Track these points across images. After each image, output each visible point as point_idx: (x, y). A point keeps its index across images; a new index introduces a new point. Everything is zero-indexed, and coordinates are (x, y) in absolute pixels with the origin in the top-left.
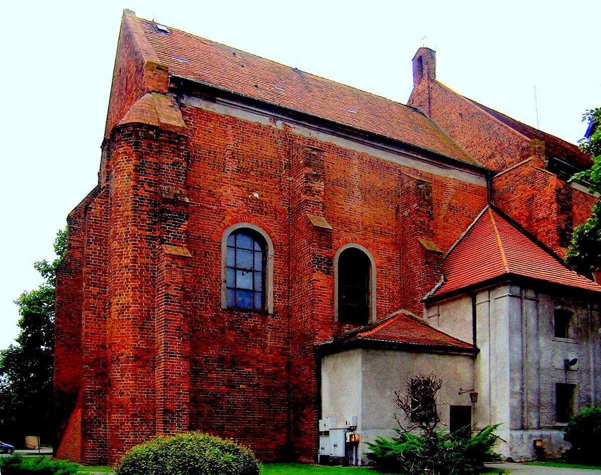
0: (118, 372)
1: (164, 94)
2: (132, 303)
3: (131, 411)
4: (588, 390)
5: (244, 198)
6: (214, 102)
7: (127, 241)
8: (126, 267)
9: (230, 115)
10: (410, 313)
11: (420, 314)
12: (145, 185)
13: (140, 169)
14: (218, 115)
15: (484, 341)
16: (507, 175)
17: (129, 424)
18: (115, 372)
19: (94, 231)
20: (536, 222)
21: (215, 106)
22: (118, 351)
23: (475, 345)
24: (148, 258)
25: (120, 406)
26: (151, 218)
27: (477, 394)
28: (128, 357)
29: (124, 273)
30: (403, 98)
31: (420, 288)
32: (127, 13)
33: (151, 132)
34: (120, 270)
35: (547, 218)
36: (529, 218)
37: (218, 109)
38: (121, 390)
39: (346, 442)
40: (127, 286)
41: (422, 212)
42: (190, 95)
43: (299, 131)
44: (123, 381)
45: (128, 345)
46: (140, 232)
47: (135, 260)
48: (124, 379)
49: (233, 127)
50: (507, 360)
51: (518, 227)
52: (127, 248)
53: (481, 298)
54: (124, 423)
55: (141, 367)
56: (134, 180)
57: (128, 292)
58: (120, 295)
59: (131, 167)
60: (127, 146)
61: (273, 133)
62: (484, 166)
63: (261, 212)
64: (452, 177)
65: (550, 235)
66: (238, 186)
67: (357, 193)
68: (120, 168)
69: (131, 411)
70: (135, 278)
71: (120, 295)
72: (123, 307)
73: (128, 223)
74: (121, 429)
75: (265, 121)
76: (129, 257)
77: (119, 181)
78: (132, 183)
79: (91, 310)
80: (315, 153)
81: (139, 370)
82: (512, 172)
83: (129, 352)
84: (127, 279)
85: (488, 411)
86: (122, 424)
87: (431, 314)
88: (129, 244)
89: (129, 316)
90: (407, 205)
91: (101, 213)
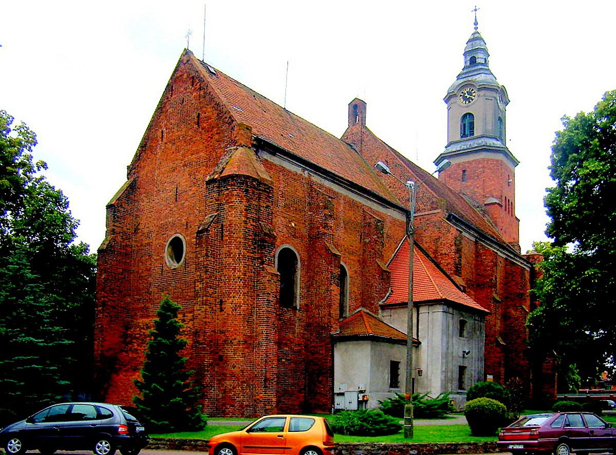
0: (232, 352)
1: (249, 148)
2: (243, 304)
3: (241, 379)
4: (472, 370)
5: (287, 226)
6: (274, 155)
7: (240, 260)
8: (239, 278)
9: (283, 166)
10: (368, 311)
11: (376, 312)
12: (251, 221)
13: (249, 209)
14: (275, 165)
15: (425, 337)
16: (421, 217)
17: (240, 388)
18: (229, 351)
19: (211, 248)
20: (440, 255)
21: (275, 158)
22: (231, 337)
23: (418, 339)
24: (251, 272)
25: (233, 375)
26: (254, 245)
27: (422, 371)
28: (239, 341)
29: (237, 282)
30: (339, 135)
31: (377, 295)
32: (187, 52)
33: (254, 183)
34: (234, 280)
35: (448, 255)
36: (435, 252)
37: (276, 160)
38: (234, 364)
39: (358, 401)
40: (240, 291)
41: (379, 242)
42: (263, 149)
43: (316, 179)
44: (235, 358)
45: (240, 333)
46: (248, 254)
47: (245, 274)
48: (236, 356)
49: (283, 175)
50: (440, 351)
51: (428, 256)
52: (240, 264)
53: (423, 310)
54: (236, 387)
55: (247, 348)
56: (245, 217)
57: (240, 295)
58: (234, 297)
59: (242, 206)
60: (240, 191)
61: (303, 179)
62: (403, 205)
63: (294, 236)
64: (389, 214)
65: (449, 266)
66: (284, 217)
67: (342, 225)
68: (234, 206)
69: (241, 379)
70: (245, 286)
71: (234, 297)
72: (236, 306)
73: (240, 247)
74: (233, 391)
75: (299, 170)
76: (241, 271)
77: (234, 215)
78: (243, 219)
79: (208, 305)
80: (330, 199)
81: (246, 350)
82: (425, 216)
83: (240, 338)
84: (239, 287)
85: (426, 383)
86: (234, 388)
87: (385, 314)
88: (241, 262)
89: (240, 312)
90: (368, 235)
91: (215, 234)
